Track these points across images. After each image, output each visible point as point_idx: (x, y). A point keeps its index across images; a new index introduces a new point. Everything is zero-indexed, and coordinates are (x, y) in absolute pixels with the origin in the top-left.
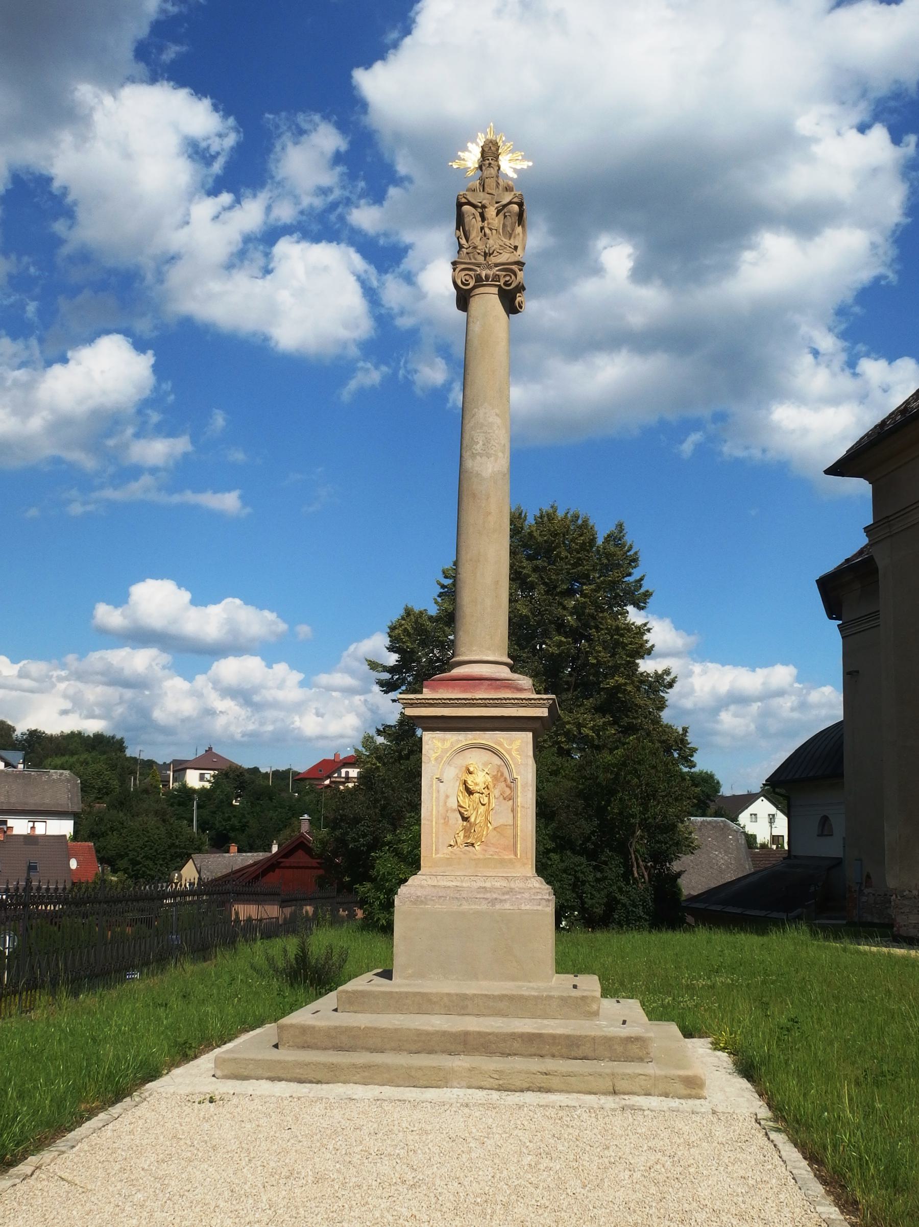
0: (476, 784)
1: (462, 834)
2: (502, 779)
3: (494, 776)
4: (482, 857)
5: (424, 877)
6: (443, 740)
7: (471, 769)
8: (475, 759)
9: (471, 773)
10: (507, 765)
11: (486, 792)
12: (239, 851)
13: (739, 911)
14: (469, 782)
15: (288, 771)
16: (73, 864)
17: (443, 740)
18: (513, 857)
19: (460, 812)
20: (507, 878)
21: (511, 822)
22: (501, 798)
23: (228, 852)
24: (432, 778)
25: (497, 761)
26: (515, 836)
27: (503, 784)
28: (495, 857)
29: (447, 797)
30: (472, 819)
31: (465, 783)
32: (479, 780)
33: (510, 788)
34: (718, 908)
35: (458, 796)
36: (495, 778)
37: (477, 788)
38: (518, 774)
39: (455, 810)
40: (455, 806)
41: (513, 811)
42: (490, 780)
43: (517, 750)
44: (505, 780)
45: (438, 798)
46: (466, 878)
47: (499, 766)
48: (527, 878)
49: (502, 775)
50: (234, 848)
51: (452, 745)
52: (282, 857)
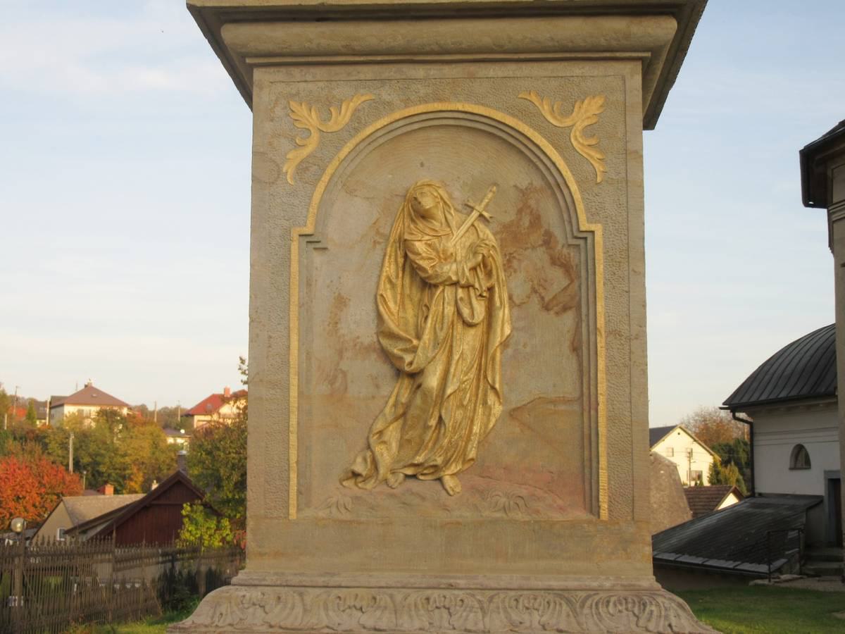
0: (447, 257)
1: (393, 434)
2: (536, 238)
3: (506, 228)
4: (468, 515)
5: (255, 594)
6: (326, 105)
7: (427, 203)
8: (441, 171)
9: (424, 216)
10: (556, 187)
11: (482, 283)
12: (116, 492)
13: (699, 561)
14: (420, 246)
15: (177, 409)
16: (662, 472)
17: (326, 105)
18: (581, 515)
19: (386, 356)
20: (563, 594)
21: (569, 388)
22: (535, 304)
23: (103, 492)
24: (287, 232)
25: (516, 174)
26: (588, 440)
27: (540, 256)
28: (519, 516)
29: (341, 302)
30: (432, 381)
31: (405, 248)
32: (454, 242)
33: (566, 267)
34: (672, 557)
35: (378, 299)
36: (511, 236)
37: (450, 270)
38: (592, 217)
39: (368, 349)
40: (367, 334)
41: (576, 349)
42: (492, 240)
43: (589, 131)
44: (548, 241)
45: (306, 307)
46: (414, 597)
47: (524, 193)
48: (640, 600)
49: (536, 221)
50: (109, 489)
51: (357, 122)
52: (155, 499)
